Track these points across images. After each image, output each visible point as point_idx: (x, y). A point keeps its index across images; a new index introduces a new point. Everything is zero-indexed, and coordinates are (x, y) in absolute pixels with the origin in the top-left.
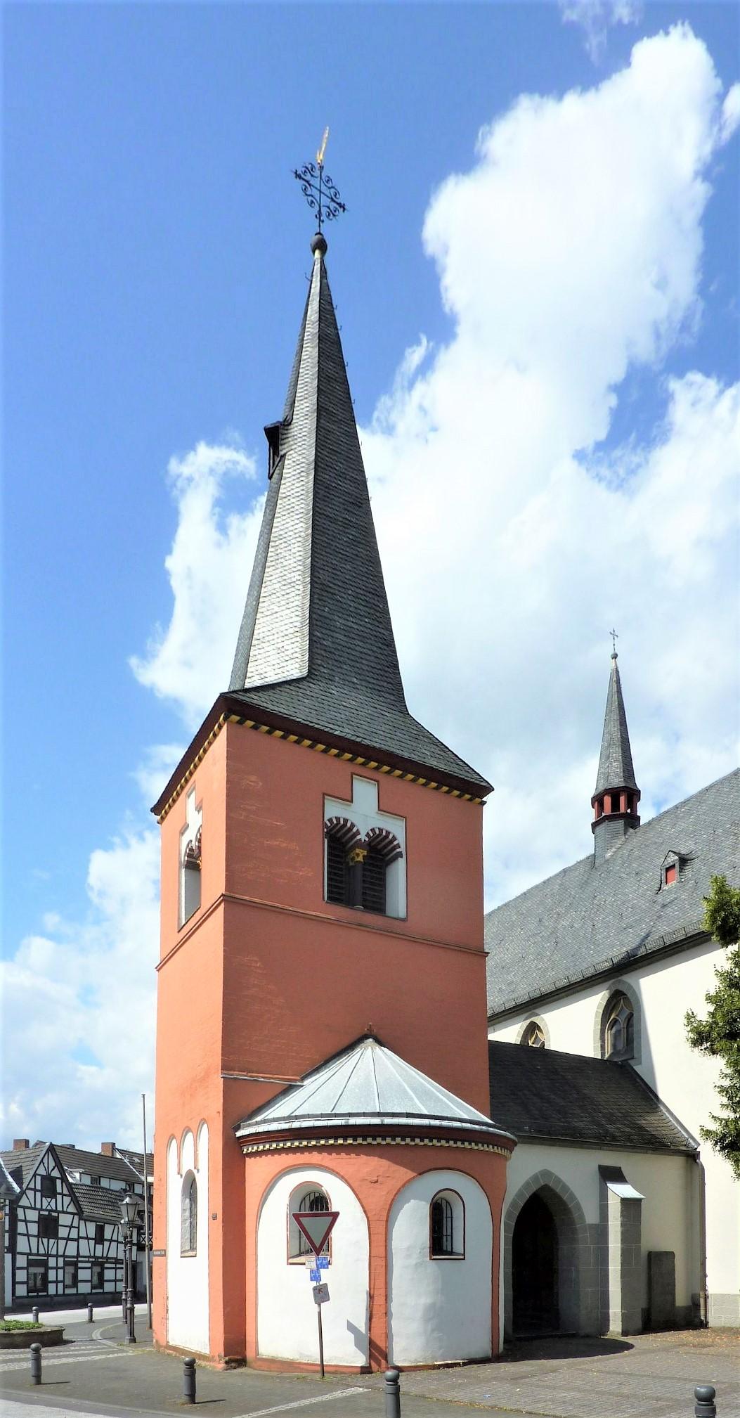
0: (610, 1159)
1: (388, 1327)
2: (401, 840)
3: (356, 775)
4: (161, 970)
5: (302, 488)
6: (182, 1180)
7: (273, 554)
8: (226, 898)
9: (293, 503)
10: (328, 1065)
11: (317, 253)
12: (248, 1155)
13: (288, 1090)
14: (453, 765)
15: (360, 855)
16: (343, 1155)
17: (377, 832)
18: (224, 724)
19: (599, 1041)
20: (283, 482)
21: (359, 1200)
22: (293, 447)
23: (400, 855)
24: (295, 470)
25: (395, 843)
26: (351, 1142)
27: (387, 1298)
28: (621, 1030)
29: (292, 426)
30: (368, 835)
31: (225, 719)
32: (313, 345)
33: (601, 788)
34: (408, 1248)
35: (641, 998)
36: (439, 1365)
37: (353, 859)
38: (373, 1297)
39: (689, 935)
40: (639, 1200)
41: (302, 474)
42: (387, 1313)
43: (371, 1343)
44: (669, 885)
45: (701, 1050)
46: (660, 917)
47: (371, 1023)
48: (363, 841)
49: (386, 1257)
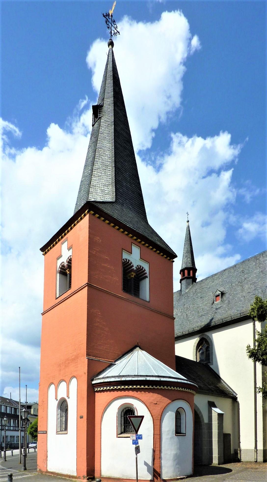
0: (212, 399)
1: (160, 463)
2: (147, 271)
3: (133, 243)
4: (44, 315)
5: (109, 131)
6: (57, 402)
7: (97, 154)
8: (88, 285)
9: (106, 136)
10: (124, 357)
11: (110, 46)
12: (97, 392)
13: (111, 365)
14: (164, 245)
15: (133, 275)
16: (143, 392)
17: (139, 267)
18: (87, 214)
19: (196, 356)
20: (100, 127)
21: (149, 411)
22: (104, 115)
23: (147, 277)
24: (106, 124)
25: (145, 272)
26: (147, 387)
27: (160, 451)
28: (204, 352)
29: (103, 107)
30: (136, 267)
31: (88, 212)
32: (111, 79)
33: (184, 267)
34: (168, 431)
35: (213, 341)
36: (179, 478)
37: (130, 276)
38: (155, 451)
39: (233, 319)
40: (223, 414)
41: (109, 125)
42: (160, 458)
43: (154, 470)
44: (217, 302)
45: (253, 359)
46: (216, 313)
47: (138, 341)
48: (135, 269)
49: (160, 435)
